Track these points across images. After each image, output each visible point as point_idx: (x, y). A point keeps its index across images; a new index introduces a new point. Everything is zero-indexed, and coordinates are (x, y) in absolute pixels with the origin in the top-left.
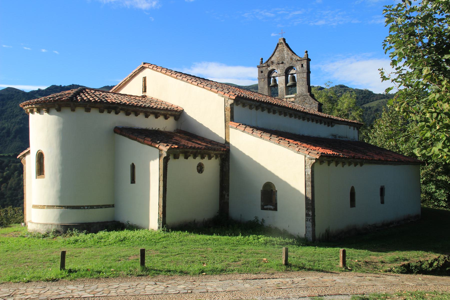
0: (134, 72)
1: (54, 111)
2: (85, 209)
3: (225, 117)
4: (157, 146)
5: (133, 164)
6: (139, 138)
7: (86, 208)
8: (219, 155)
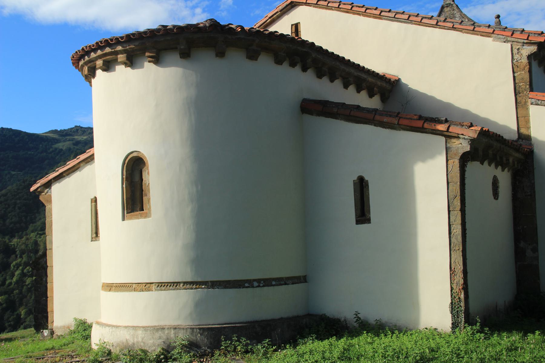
0: (270, 15)
1: (175, 57)
2: (253, 287)
3: (517, 117)
7: (256, 284)
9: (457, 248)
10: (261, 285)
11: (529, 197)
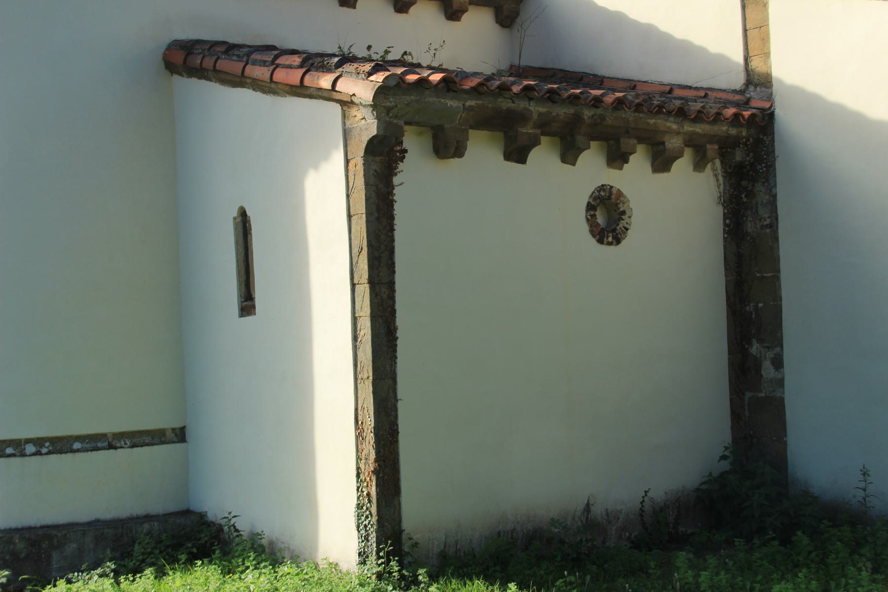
2: (23, 455)
3: (745, 31)
4: (325, 82)
5: (243, 214)
6: (254, 63)
7: (30, 449)
8: (712, 149)
9: (365, 376)
10: (44, 450)
11: (768, 231)
